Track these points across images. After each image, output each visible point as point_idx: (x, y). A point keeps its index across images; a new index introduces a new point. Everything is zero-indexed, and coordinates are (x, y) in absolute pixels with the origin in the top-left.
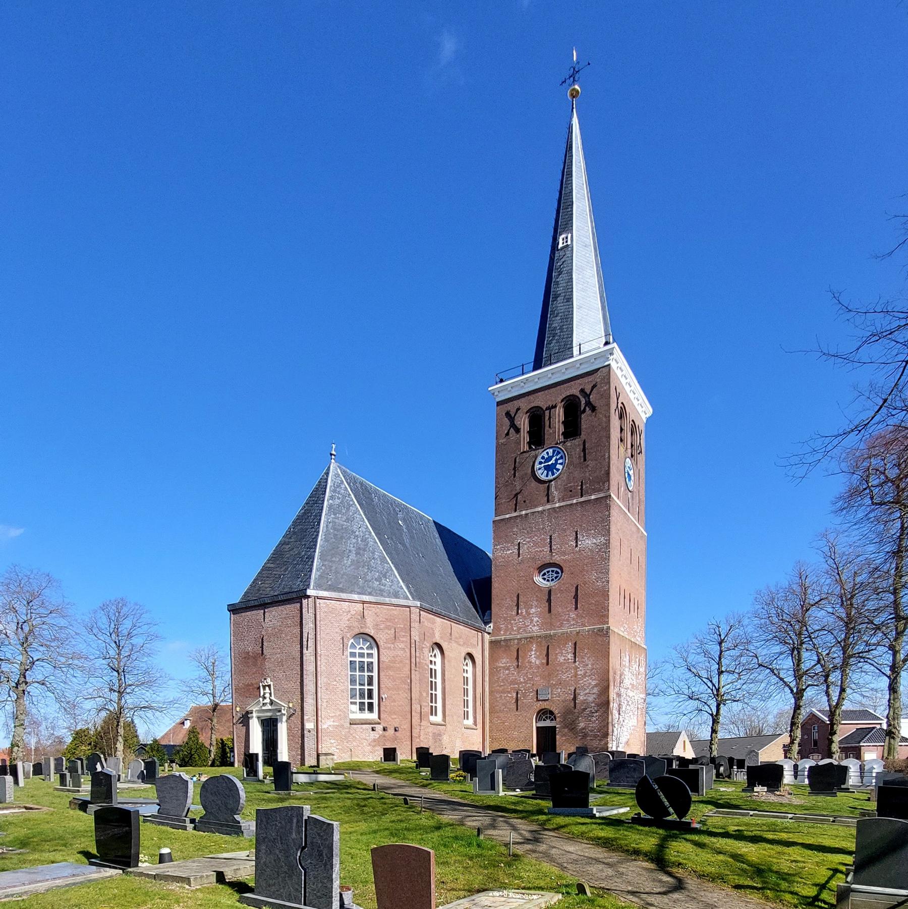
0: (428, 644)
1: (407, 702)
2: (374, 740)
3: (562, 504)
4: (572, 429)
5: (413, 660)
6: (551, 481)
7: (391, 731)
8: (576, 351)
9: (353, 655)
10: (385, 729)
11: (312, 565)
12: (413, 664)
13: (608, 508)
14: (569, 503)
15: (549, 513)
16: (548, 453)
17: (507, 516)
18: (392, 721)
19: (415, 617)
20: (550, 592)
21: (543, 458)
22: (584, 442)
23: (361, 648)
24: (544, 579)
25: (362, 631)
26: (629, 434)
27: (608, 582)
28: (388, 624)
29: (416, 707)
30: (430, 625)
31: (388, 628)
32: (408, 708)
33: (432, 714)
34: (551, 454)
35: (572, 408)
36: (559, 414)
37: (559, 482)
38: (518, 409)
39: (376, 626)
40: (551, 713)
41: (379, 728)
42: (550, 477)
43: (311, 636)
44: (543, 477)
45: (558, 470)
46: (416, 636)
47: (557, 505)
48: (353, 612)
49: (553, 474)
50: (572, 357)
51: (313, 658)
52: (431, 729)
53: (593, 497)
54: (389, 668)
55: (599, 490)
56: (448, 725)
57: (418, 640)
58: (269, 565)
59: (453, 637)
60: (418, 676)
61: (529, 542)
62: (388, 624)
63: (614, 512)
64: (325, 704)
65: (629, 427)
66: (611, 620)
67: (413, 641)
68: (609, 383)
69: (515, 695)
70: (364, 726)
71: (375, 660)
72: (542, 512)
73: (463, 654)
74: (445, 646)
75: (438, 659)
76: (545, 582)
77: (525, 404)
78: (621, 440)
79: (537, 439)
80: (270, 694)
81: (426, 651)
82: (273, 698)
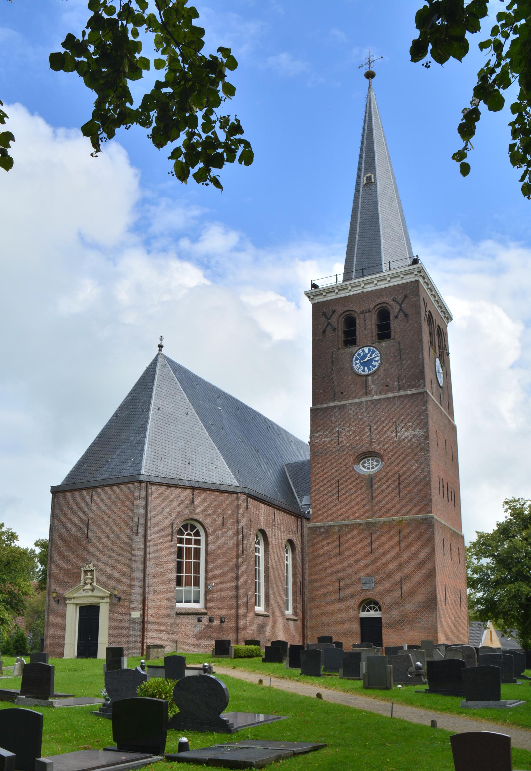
0: (254, 531)
1: (233, 591)
2: (200, 632)
3: (379, 397)
4: (384, 332)
5: (240, 547)
6: (367, 376)
7: (217, 623)
8: (385, 267)
9: (181, 541)
10: (211, 620)
11: (142, 450)
12: (240, 551)
13: (425, 403)
14: (386, 396)
15: (367, 405)
16: (363, 351)
17: (325, 406)
18: (221, 611)
19: (242, 503)
20: (372, 479)
21: (359, 355)
22: (399, 343)
23: (189, 534)
24: (364, 467)
25: (191, 517)
26: (436, 337)
27: (429, 472)
28: (217, 510)
29: (242, 596)
30: (256, 512)
31: (217, 514)
32: (234, 598)
33: (256, 605)
34: (366, 352)
35: (384, 316)
36: (372, 320)
37: (376, 377)
38: (334, 311)
39: (205, 513)
40: (376, 603)
41: (205, 619)
42: (367, 372)
43: (142, 521)
44: (360, 371)
45: (374, 366)
46: (243, 523)
47: (375, 398)
48: (183, 498)
49: (369, 370)
50: (382, 272)
51: (142, 544)
52: (257, 620)
53: (410, 392)
54: (217, 555)
55: (415, 387)
56: (271, 617)
57: (245, 527)
58: (95, 448)
59: (276, 523)
60: (245, 563)
61: (348, 431)
62: (217, 510)
63: (430, 407)
64: (152, 593)
65: (436, 330)
66: (434, 509)
67: (240, 528)
68: (418, 295)
69: (337, 584)
70: (190, 617)
71: (202, 547)
72: (360, 404)
73: (285, 541)
74: (269, 532)
75: (261, 547)
76: (365, 470)
77: (340, 310)
78: (431, 343)
79: (350, 338)
80: (92, 579)
81: (253, 539)
82: (95, 584)
